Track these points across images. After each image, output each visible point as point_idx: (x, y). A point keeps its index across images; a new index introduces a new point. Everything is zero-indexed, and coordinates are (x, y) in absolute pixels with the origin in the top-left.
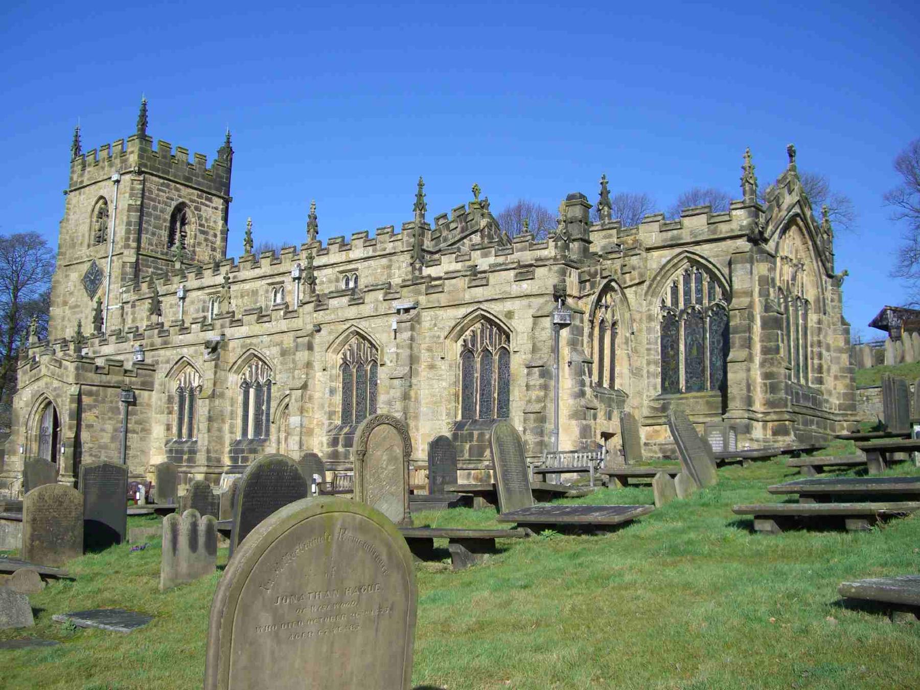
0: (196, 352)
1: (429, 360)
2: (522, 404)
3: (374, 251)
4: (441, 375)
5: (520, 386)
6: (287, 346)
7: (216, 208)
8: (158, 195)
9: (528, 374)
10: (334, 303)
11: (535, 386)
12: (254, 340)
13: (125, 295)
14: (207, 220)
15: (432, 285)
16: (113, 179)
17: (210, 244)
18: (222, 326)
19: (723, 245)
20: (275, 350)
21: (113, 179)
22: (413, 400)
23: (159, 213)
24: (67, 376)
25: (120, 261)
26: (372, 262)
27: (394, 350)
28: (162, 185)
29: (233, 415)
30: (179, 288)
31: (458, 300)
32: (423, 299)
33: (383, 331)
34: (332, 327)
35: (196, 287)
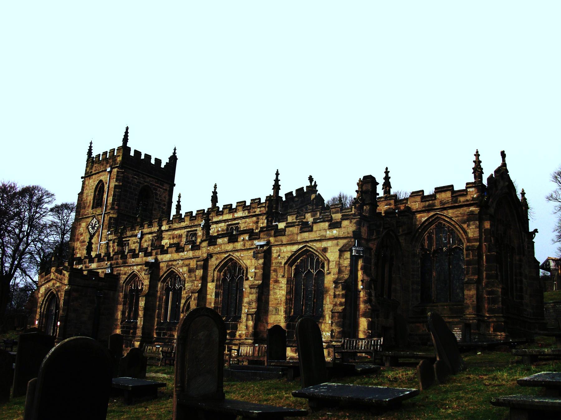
0: (141, 268)
1: (275, 277)
2: (331, 306)
3: (249, 213)
4: (281, 287)
5: (330, 295)
6: (192, 266)
7: (166, 190)
8: (132, 180)
9: (335, 287)
10: (220, 241)
11: (339, 295)
12: (174, 263)
13: (110, 236)
14: (160, 196)
15: (280, 233)
16: (107, 171)
17: (161, 210)
18: (157, 254)
19: (461, 210)
20: (185, 269)
21: (107, 171)
22: (263, 301)
23: (132, 191)
24: (65, 280)
25: (109, 216)
26: (247, 220)
27: (253, 270)
28: (135, 175)
29: (160, 307)
30: (139, 232)
31: (294, 240)
32: (272, 239)
33: (248, 259)
34: (218, 256)
35: (148, 232)
